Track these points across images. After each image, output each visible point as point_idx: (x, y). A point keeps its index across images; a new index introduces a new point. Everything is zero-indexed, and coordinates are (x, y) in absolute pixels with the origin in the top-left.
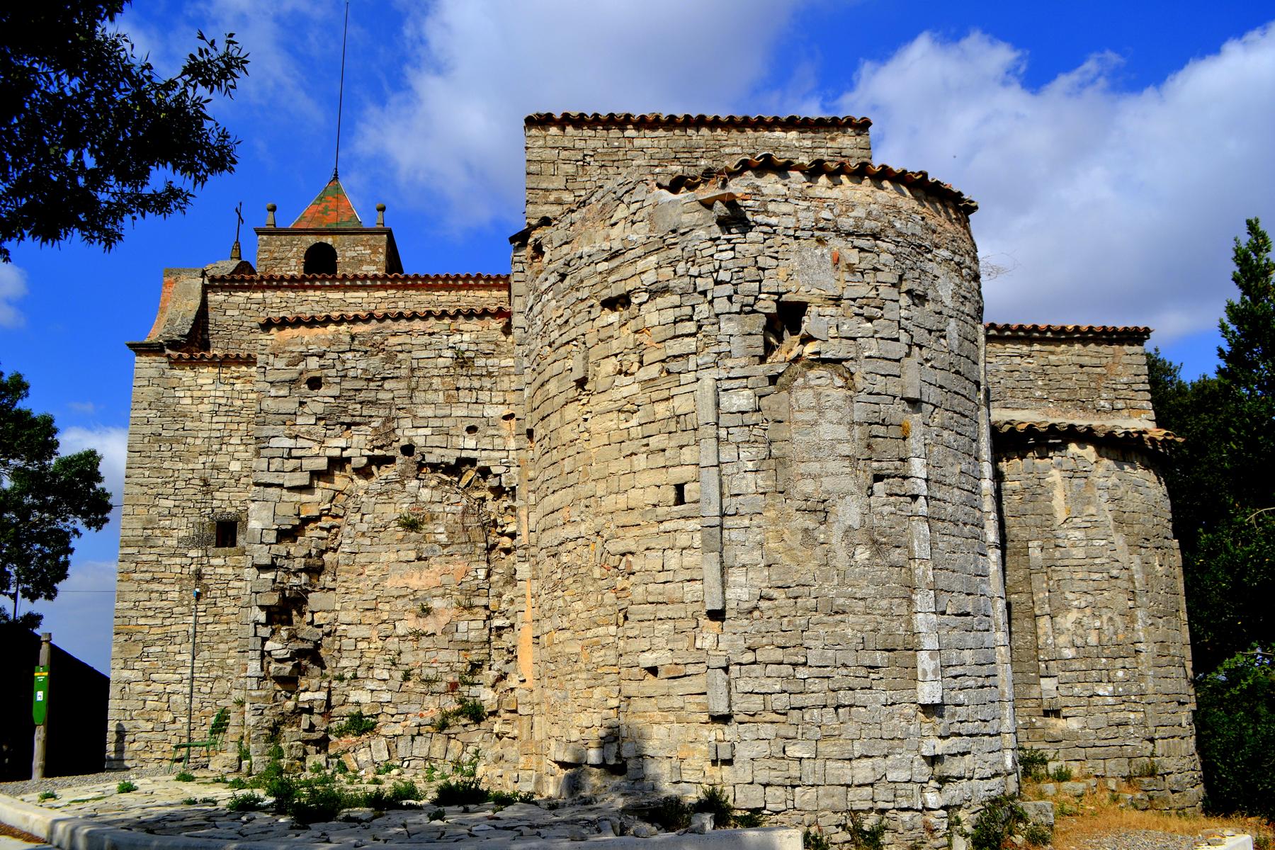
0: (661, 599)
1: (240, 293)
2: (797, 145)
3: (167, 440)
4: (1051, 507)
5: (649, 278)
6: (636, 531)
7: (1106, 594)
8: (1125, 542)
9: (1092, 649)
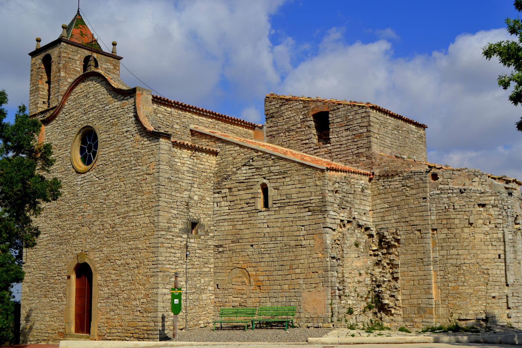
0: (496, 281)
1: (162, 106)
3: (174, 182)
5: (492, 202)
6: (489, 264)
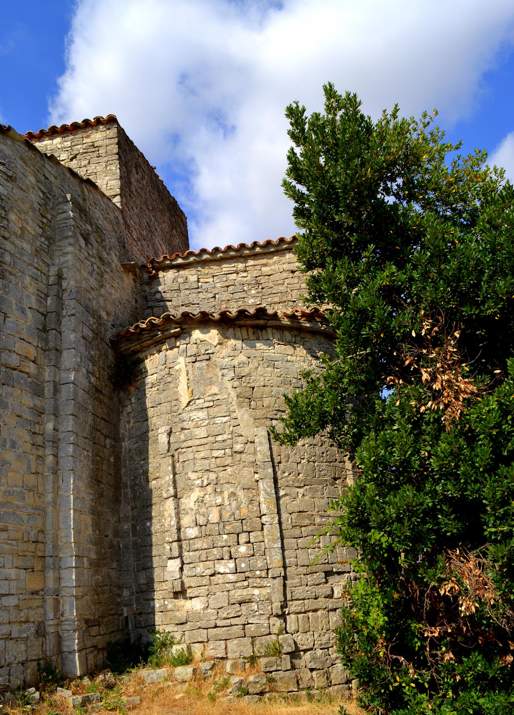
2: (60, 147)
4: (176, 393)
7: (229, 469)
8: (251, 416)
9: (213, 526)
